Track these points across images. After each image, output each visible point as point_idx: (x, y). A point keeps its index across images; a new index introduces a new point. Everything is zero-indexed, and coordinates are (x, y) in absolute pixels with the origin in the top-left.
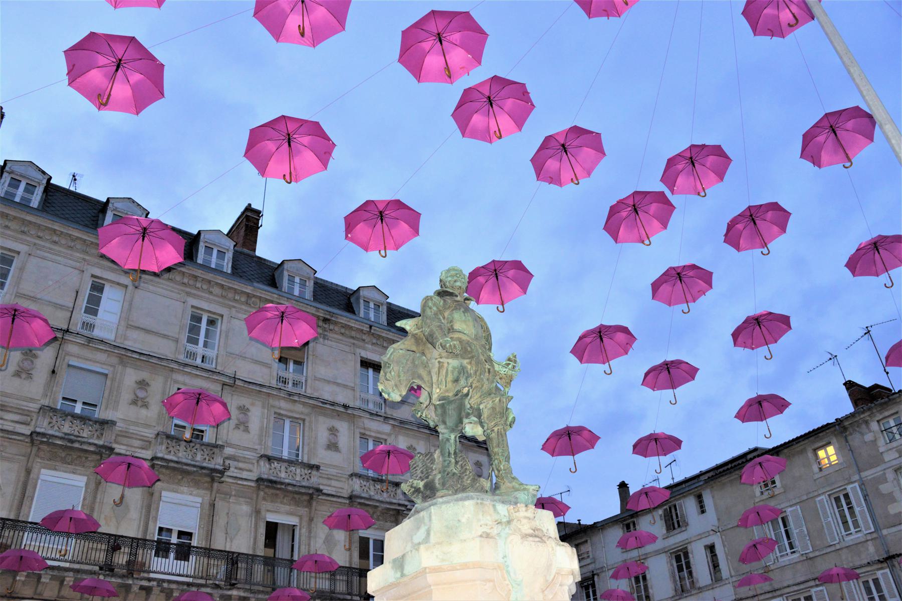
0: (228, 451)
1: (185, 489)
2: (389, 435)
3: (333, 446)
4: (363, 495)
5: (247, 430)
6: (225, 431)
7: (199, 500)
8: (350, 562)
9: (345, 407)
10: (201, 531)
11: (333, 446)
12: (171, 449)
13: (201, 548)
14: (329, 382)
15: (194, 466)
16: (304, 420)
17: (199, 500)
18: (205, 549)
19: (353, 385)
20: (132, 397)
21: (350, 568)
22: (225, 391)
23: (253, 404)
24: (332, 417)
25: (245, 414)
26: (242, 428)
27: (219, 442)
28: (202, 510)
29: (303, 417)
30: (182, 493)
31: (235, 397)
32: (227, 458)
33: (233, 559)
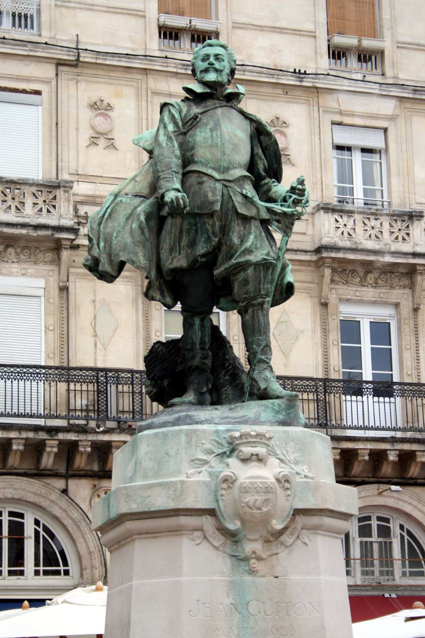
0: (82, 189)
1: (15, 268)
2: (392, 118)
3: (101, 138)
4: (341, 244)
5: (111, 145)
6: (73, 153)
7: (222, 314)
8: (326, 369)
9: (299, 74)
10: (51, 335)
11: (101, 138)
12: (10, 203)
13: (50, 368)
14: (261, 28)
15: (24, 226)
16: (386, 130)
17: (41, 283)
18: (62, 368)
19: (310, 27)
20: (91, 133)
21: (326, 380)
22: (63, 76)
23: (118, 95)
24: (274, 98)
25: (106, 116)
26: (102, 142)
27: (65, 176)
28: (47, 300)
29: (383, 124)
30: (10, 274)
31: (82, 86)
32: (82, 203)
33: (102, 377)
